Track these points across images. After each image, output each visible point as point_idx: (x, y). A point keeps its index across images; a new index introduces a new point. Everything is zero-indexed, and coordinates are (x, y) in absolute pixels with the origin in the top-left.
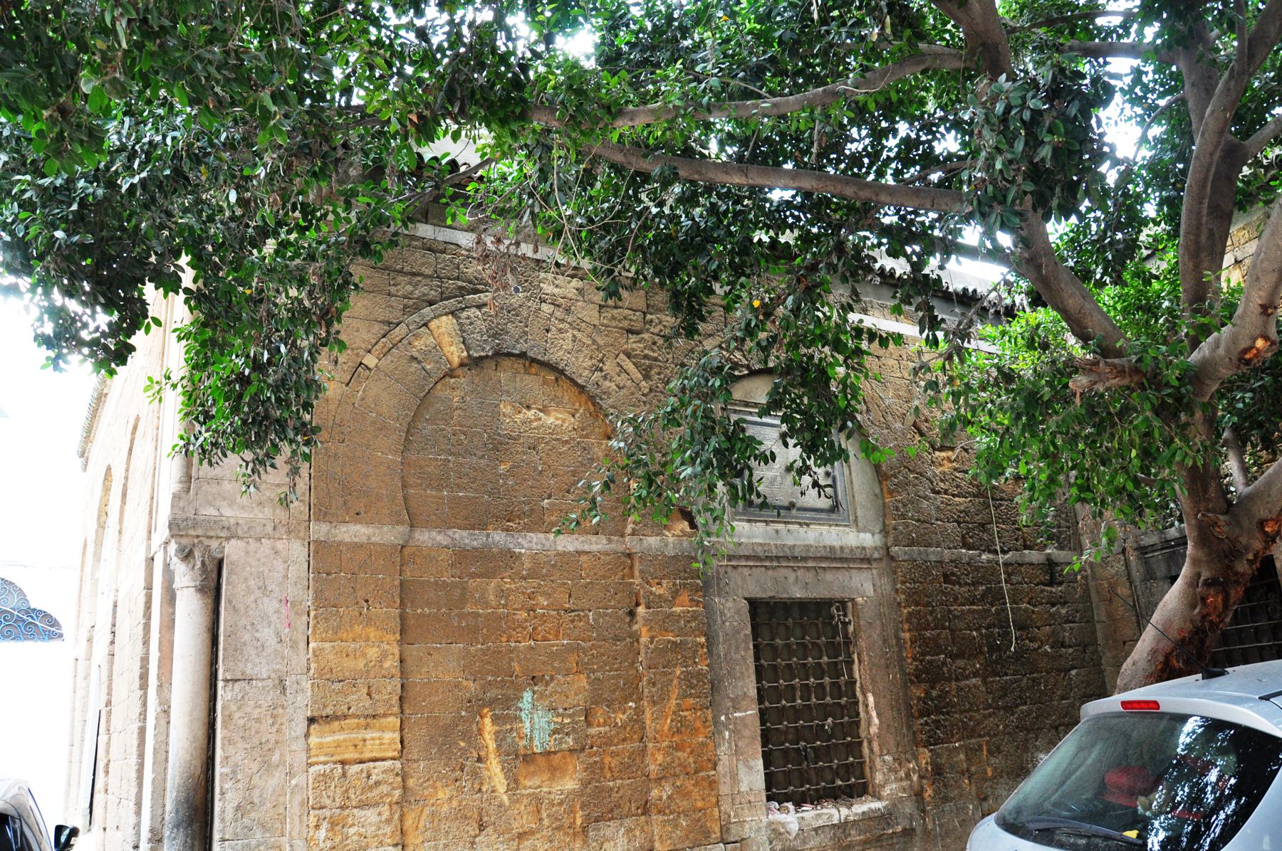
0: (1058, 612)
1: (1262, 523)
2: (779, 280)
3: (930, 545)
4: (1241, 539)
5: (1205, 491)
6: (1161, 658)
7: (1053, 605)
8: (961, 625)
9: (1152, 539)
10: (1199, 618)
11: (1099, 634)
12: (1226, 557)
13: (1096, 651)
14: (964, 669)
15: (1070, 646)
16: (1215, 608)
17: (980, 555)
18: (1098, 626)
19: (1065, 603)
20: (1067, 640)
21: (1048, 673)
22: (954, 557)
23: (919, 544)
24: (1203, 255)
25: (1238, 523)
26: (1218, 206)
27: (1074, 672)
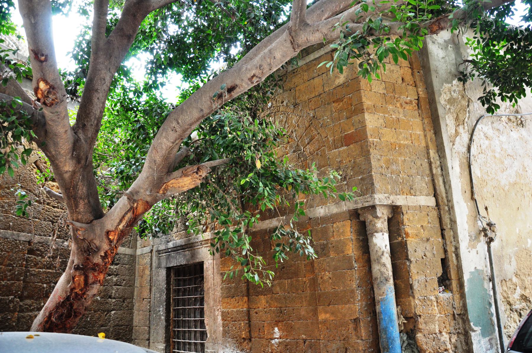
0: (112, 279)
1: (108, 233)
2: (213, 150)
3: (23, 231)
4: (95, 242)
5: (77, 206)
6: (47, 314)
7: (109, 275)
8: (36, 280)
9: (162, 247)
10: (69, 290)
11: (135, 293)
12: (85, 252)
13: (132, 302)
14: (30, 306)
15: (114, 298)
16: (79, 284)
17: (63, 242)
18: (136, 289)
19: (117, 275)
20: (113, 295)
21: (95, 311)
22: (42, 241)
23: (14, 229)
24: (101, 53)
25: (93, 231)
26: (123, 29)
27: (113, 312)
